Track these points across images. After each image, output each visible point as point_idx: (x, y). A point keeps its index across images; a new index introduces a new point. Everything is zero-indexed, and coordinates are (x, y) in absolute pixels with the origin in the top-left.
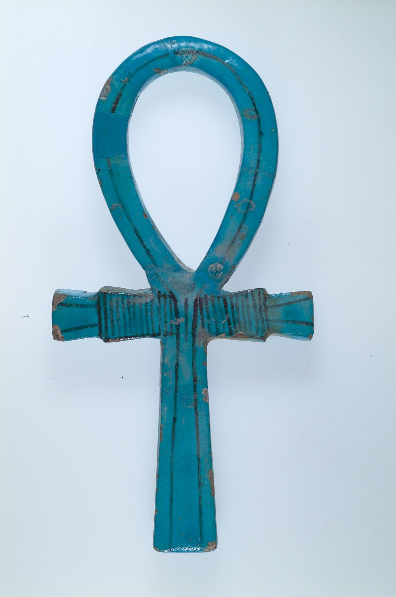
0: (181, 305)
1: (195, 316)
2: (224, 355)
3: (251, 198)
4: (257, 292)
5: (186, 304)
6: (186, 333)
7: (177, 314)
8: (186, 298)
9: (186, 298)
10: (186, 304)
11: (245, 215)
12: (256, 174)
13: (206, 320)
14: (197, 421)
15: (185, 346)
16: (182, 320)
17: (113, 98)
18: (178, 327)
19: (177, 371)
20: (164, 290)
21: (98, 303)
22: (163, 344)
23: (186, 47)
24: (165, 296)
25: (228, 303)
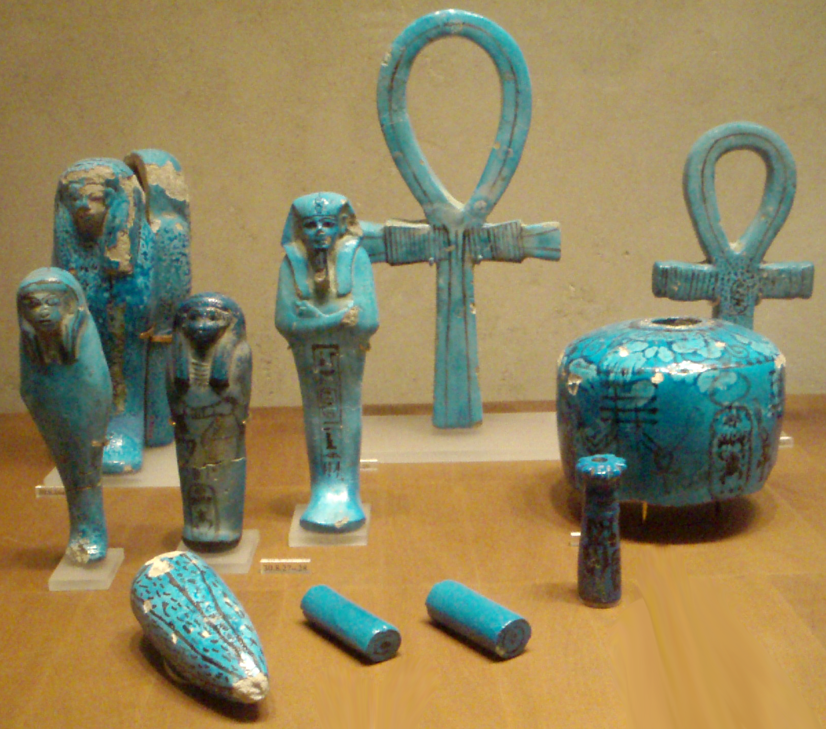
0: (452, 237)
1: (464, 245)
2: (487, 276)
3: (509, 147)
4: (708, 277)
5: (457, 235)
6: (457, 258)
7: (449, 243)
8: (456, 232)
9: (456, 232)
10: (457, 235)
11: (505, 161)
12: (514, 126)
13: (473, 247)
14: (466, 328)
15: (457, 270)
16: (453, 248)
17: (394, 65)
18: (450, 253)
19: (449, 289)
20: (439, 224)
21: (385, 236)
22: (295, 409)
23: (457, 16)
24: (439, 229)
25: (490, 238)
